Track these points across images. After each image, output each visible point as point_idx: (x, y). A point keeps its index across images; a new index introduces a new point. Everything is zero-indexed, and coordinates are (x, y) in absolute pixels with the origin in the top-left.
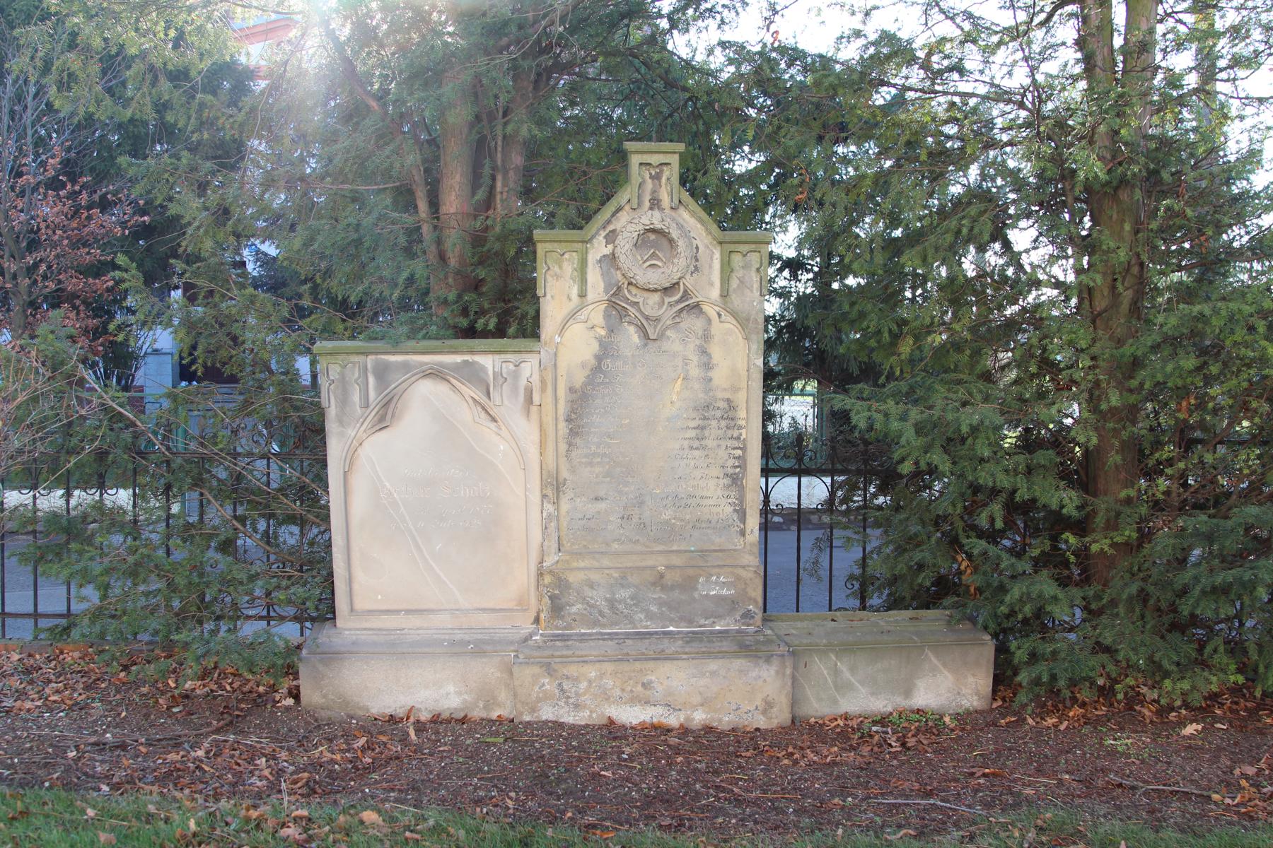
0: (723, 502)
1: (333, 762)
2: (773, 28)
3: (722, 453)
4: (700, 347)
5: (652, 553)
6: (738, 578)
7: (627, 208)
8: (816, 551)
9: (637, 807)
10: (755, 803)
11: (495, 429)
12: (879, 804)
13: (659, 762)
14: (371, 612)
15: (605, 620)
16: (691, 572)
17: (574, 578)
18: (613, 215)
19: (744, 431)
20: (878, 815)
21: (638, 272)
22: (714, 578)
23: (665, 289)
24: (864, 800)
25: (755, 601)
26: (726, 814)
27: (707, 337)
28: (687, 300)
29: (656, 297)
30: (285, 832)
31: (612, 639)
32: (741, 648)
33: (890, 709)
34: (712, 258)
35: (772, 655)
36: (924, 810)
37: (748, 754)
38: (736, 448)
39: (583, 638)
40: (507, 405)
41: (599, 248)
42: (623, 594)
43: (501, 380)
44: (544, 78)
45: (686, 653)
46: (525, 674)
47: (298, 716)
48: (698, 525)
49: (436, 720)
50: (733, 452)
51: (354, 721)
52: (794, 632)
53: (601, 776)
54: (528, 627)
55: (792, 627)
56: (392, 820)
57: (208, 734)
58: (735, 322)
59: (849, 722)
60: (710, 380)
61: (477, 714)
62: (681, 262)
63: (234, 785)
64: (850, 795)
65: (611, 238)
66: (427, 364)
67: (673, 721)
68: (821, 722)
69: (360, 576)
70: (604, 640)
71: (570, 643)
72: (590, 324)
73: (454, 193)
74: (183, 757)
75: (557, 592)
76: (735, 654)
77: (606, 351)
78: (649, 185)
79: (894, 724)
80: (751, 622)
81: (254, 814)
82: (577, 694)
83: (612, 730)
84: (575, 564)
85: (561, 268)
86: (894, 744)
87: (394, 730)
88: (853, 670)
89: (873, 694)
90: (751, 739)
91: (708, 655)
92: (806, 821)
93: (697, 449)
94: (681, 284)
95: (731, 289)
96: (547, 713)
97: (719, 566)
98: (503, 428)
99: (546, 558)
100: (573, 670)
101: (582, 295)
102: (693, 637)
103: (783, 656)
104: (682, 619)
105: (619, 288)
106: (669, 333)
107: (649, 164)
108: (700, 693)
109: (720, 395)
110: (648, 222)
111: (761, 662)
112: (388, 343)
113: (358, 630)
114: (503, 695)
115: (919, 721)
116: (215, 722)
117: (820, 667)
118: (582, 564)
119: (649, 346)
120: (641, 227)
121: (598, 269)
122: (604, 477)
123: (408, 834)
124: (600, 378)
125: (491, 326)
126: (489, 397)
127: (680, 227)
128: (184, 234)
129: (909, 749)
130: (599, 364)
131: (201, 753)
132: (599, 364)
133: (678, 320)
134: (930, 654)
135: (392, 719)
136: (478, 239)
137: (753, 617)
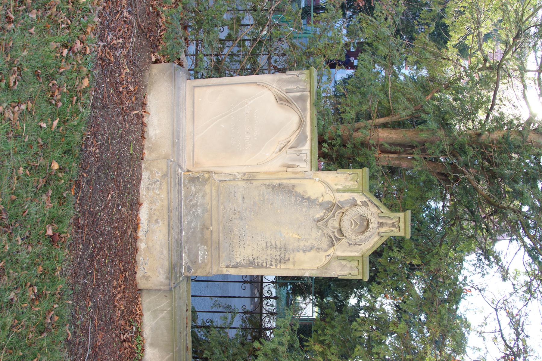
0: (242, 258)
1: (120, 74)
2: (473, 290)
3: (264, 257)
4: (314, 247)
5: (218, 224)
6: (206, 265)
7: (379, 211)
8: (225, 306)
9: (90, 208)
10: (91, 264)
11: (275, 151)
12: (89, 324)
13: (116, 223)
14: (193, 95)
15: (188, 202)
16: (209, 242)
17: (207, 188)
18: (375, 205)
19: (274, 267)
20: (82, 323)
21: (348, 216)
22: (206, 253)
23: (341, 230)
24: (91, 317)
25: (195, 273)
26: (84, 250)
27: (319, 250)
28: (336, 240)
29: (337, 226)
30: (78, 43)
31: (178, 205)
32: (173, 265)
33: (145, 336)
34: (355, 252)
35: (170, 280)
36: (84, 346)
37: (121, 266)
38: (266, 264)
39: (180, 192)
40: (287, 156)
41: (359, 198)
42: (200, 211)
43: (298, 153)
44: (443, 178)
45: (171, 239)
46: (163, 165)
47: (146, 62)
48: (231, 246)
49: (144, 125)
50: (265, 262)
51: (143, 87)
52: (181, 291)
53: (109, 194)
54: (186, 167)
55: (184, 290)
56: (84, 92)
57: (137, 20)
58: (325, 263)
59: (138, 316)
60: (298, 251)
61: (146, 143)
62: (353, 237)
63: (108, 26)
64: (95, 311)
65: (365, 204)
66: (306, 120)
67: (141, 233)
68: (139, 303)
69: (210, 90)
70: (178, 201)
71: (177, 186)
72: (324, 194)
73: (388, 135)
74: (124, 6)
75: (201, 180)
76: (170, 263)
77: (312, 202)
78: (390, 222)
79: (136, 337)
80: (186, 271)
81: (89, 30)
82: (154, 189)
83: (136, 205)
84: (213, 188)
85: (350, 180)
86: (125, 336)
87: (139, 105)
88: (163, 318)
89: (152, 328)
90: (130, 269)
91: (170, 250)
92: (79, 288)
93: (266, 245)
94: (343, 237)
95: (341, 261)
96: (145, 175)
97: (212, 255)
98: (276, 155)
99: (216, 174)
100: (164, 186)
101: (338, 191)
102: (179, 244)
103: (169, 285)
104: (188, 238)
105: (341, 208)
106: (320, 231)
107: (399, 222)
108: (153, 246)
109: (291, 256)
110: (372, 221)
111: (167, 274)
112: (315, 101)
113: (186, 90)
114: (154, 155)
115: (138, 349)
116: (143, 24)
117: (164, 303)
118: (213, 191)
119: (314, 222)
120: (370, 218)
121: (350, 198)
122: (253, 201)
123: (75, 98)
124: (299, 199)
125: (324, 149)
126: (290, 148)
127: (370, 237)
128: (369, 15)
129: (122, 343)
130: (306, 199)
131: (125, 14)
132: (306, 199)
133: (326, 236)
134: (170, 356)
135: (144, 105)
136: (364, 144)
137: (188, 271)
